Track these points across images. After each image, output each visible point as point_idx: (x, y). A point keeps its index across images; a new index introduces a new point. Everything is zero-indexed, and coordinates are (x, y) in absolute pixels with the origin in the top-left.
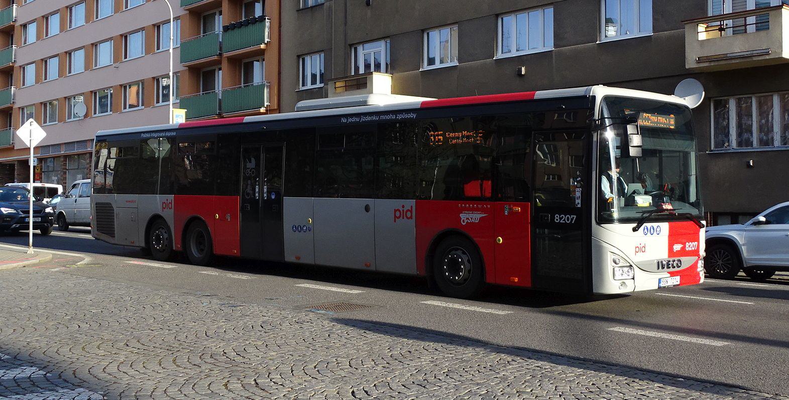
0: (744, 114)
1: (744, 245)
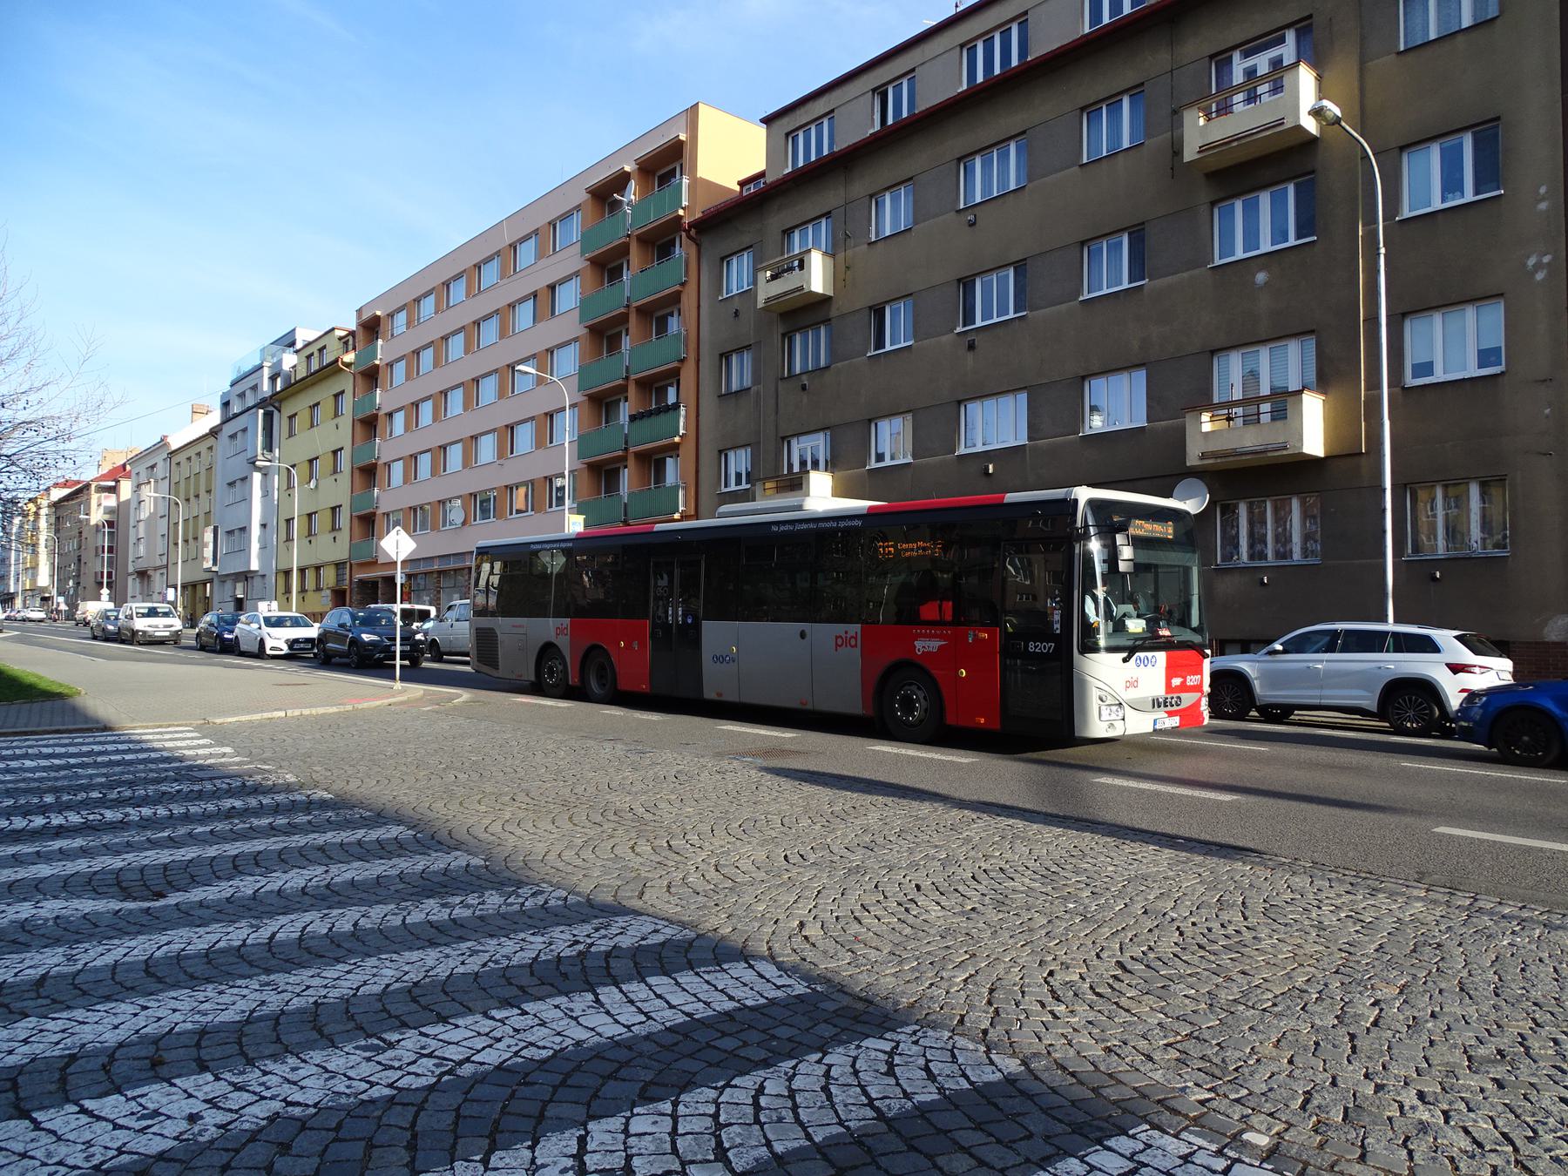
0: (1256, 521)
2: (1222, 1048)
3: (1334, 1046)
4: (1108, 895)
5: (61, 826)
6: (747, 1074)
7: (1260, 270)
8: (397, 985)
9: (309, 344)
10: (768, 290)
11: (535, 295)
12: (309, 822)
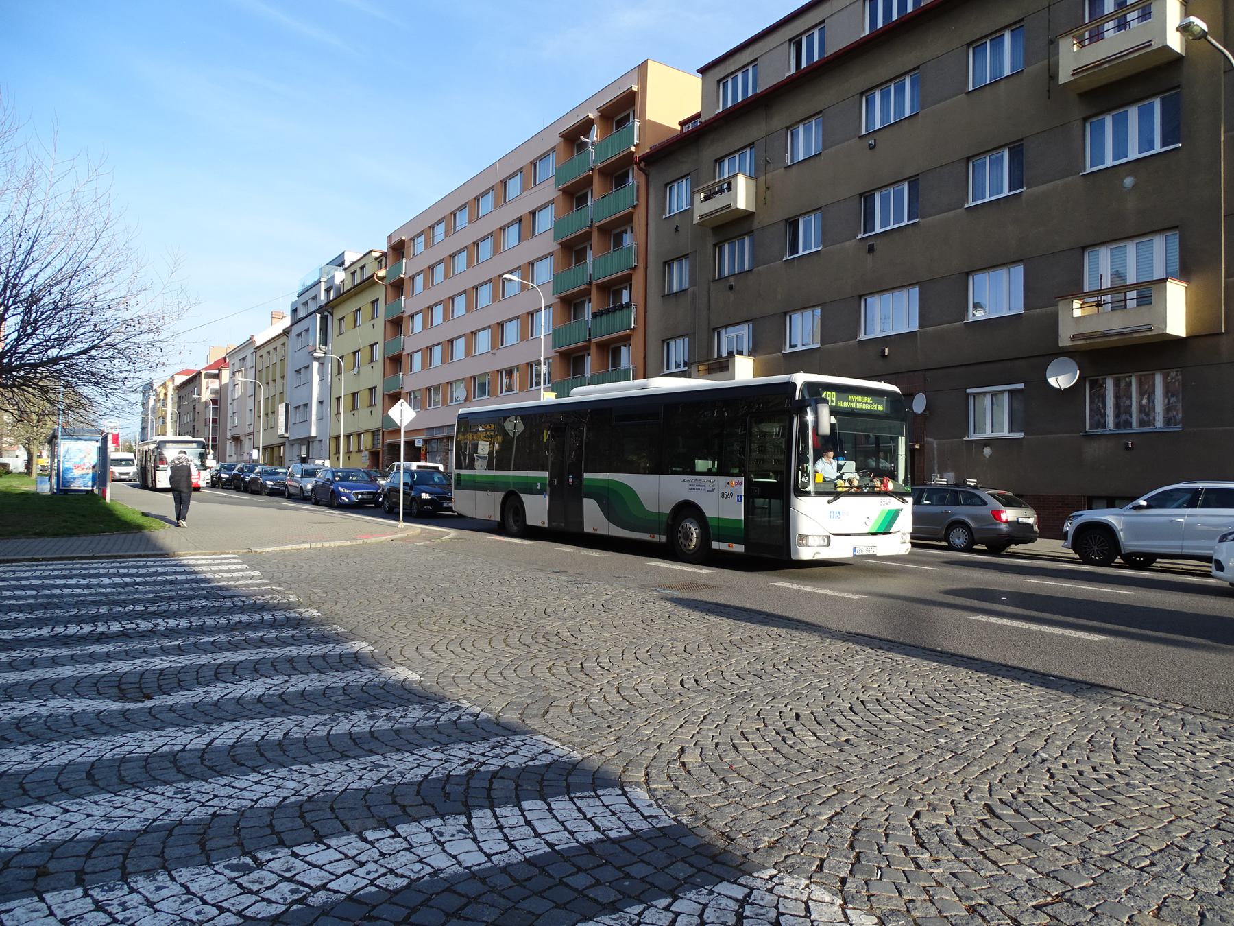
0: (1122, 395)
1: (1121, 530)
2: (1096, 915)
3: (1221, 919)
4: (980, 731)
5: (103, 633)
6: (591, 919)
7: (1128, 176)
8: (293, 799)
9: (353, 264)
10: (702, 208)
11: (520, 220)
12: (293, 636)
